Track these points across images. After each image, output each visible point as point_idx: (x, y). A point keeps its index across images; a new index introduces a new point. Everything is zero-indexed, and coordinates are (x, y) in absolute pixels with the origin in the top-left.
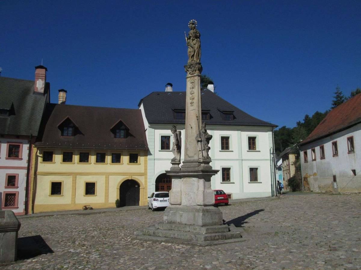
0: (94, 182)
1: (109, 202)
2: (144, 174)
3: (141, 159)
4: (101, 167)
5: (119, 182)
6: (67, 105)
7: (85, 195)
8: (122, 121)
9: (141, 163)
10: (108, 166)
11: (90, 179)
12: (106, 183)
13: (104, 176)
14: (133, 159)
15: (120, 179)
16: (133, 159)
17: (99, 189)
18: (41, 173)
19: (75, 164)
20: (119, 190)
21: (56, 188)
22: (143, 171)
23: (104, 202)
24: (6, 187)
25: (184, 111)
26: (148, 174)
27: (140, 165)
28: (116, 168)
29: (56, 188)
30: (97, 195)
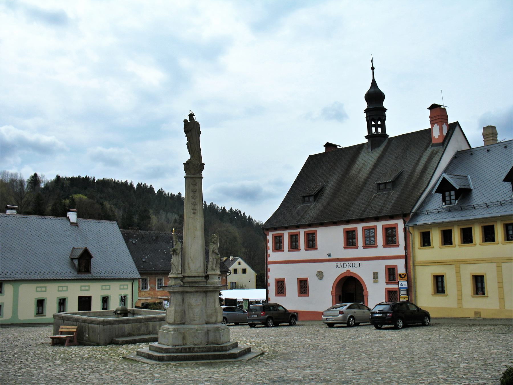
1: (506, 308)
11: (478, 270)
13: (494, 265)
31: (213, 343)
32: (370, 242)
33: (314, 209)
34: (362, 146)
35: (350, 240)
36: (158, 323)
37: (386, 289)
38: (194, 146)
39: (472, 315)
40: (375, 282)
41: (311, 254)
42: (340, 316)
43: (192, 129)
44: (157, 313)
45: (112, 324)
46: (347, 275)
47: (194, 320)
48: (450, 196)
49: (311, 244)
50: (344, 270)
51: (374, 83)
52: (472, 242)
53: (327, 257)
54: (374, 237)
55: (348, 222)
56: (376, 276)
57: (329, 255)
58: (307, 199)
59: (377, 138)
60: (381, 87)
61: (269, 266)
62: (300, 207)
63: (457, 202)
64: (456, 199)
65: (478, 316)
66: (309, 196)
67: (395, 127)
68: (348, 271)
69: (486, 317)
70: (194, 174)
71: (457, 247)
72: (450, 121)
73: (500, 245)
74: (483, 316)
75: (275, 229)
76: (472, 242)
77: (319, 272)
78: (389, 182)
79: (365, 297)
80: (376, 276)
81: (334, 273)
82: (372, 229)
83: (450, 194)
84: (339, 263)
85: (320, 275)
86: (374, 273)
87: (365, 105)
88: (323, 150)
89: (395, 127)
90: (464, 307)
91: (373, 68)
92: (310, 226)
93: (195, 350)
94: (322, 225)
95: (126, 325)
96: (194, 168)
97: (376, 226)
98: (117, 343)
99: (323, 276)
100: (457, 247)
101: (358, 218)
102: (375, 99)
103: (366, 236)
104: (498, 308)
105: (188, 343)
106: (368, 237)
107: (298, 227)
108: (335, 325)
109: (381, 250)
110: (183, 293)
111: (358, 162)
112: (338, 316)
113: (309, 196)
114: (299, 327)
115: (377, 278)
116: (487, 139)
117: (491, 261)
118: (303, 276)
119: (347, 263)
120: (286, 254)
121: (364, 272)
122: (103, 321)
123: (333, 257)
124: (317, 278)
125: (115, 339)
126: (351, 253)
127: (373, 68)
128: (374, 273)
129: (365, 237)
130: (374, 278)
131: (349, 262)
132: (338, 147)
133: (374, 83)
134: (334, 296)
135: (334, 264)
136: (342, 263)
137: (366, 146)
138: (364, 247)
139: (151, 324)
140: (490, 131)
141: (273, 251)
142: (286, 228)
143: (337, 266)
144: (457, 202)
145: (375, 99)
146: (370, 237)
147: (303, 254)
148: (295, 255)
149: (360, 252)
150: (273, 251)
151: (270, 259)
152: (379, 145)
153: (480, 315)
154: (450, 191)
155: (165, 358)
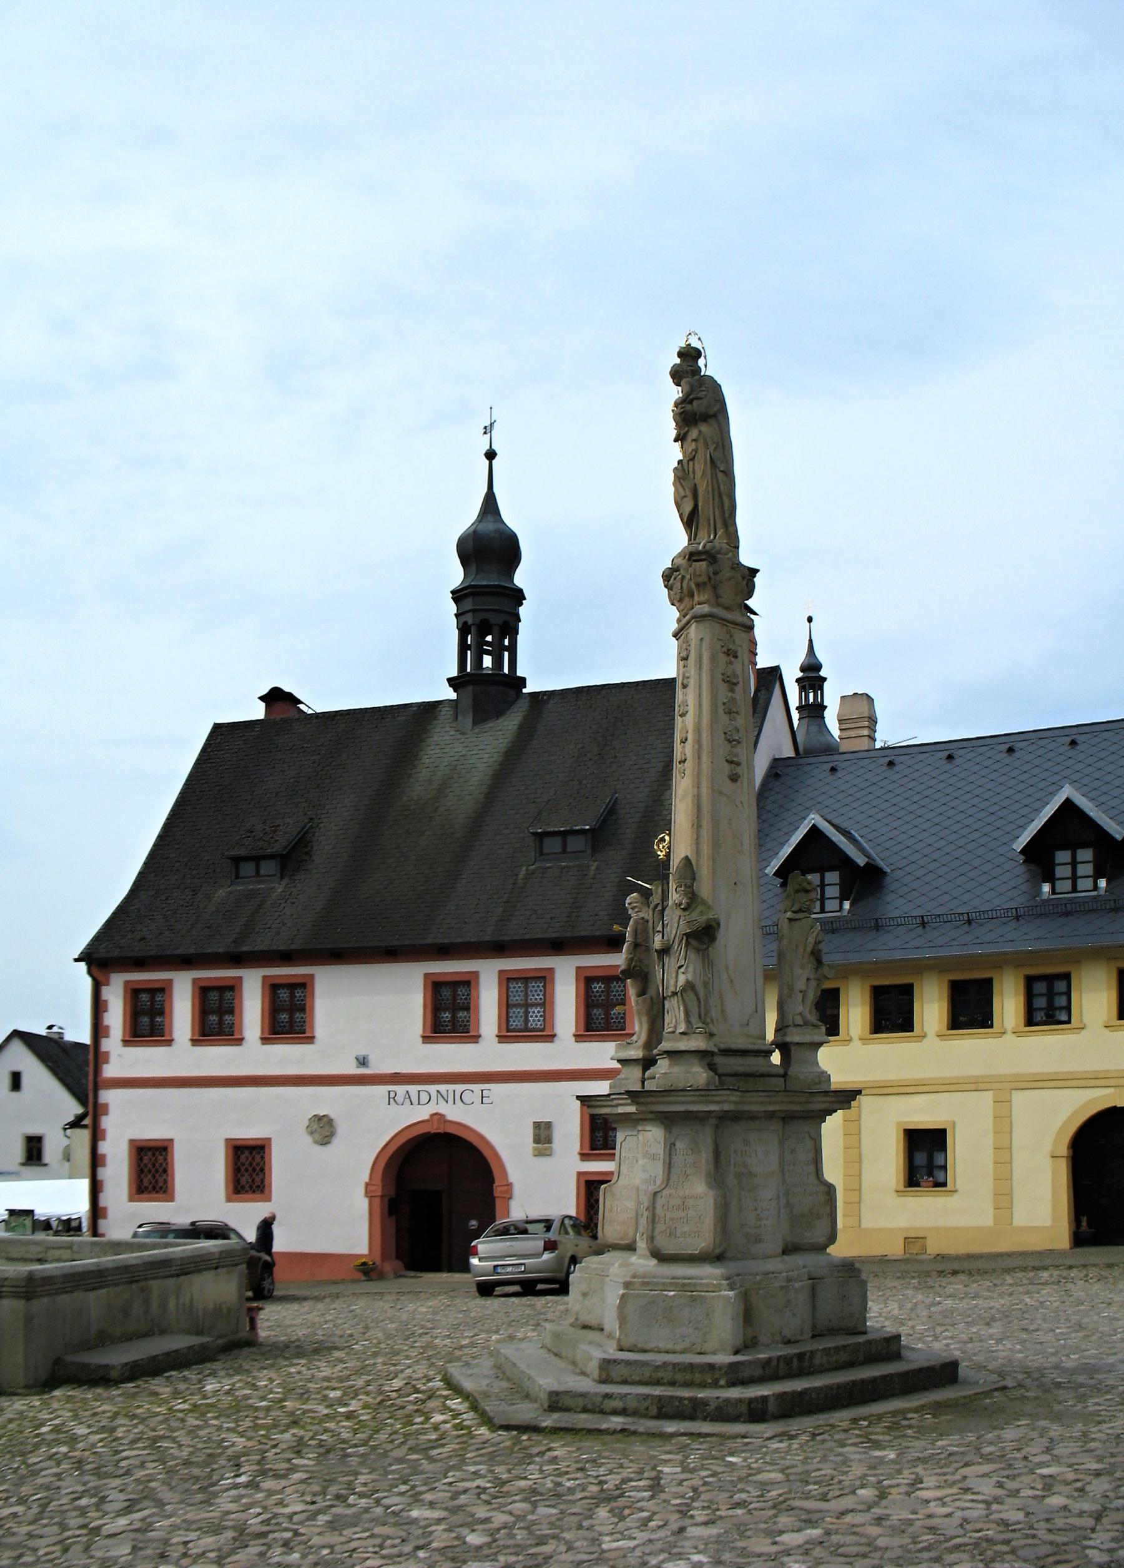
0: (901, 1135)
1: (1015, 1223)
4: (972, 1050)
5: (1065, 1125)
6: (893, 756)
7: (901, 1188)
8: (824, 826)
9: (1087, 1019)
10: (1010, 1045)
11: (924, 1113)
12: (997, 1132)
13: (988, 1096)
15: (1073, 1107)
17: (965, 1156)
18: (941, 1082)
19: (926, 1040)
20: (1063, 1169)
21: (925, 1155)
23: (989, 1222)
24: (584, 1157)
25: (844, 727)
27: (1083, 1032)
28: (1046, 1049)
29: (925, 1155)
30: (958, 1186)
31: (833, 1331)
32: (526, 1021)
33: (291, 906)
34: (431, 708)
35: (448, 1015)
36: (171, 1282)
37: (579, 1174)
38: (707, 489)
39: (895, 1249)
40: (539, 1154)
41: (286, 1057)
42: (547, 1256)
43: (701, 410)
44: (185, 1244)
45: (58, 1292)
46: (434, 1129)
47: (758, 1240)
48: (1074, 864)
49: (289, 1019)
50: (422, 1113)
51: (490, 505)
52: (910, 1028)
53: (353, 1070)
54: (543, 1005)
55: (444, 951)
56: (543, 1134)
57: (363, 1062)
58: (247, 869)
59: (487, 687)
60: (511, 517)
61: (108, 1096)
62: (222, 892)
63: (847, 905)
64: (843, 898)
65: (915, 1249)
66: (257, 859)
67: (549, 658)
68: (438, 1117)
69: (943, 1251)
70: (728, 609)
71: (856, 1043)
72: (763, 662)
73: (931, 1041)
74: (933, 1248)
75: (140, 964)
76: (910, 1028)
77: (319, 1118)
78: (582, 832)
79: (498, 1202)
80: (543, 1134)
81: (377, 1122)
82: (536, 978)
83: (1074, 857)
84: (401, 1089)
85: (323, 1129)
86: (537, 1125)
87: (455, 575)
88: (258, 711)
89: (549, 658)
90: (864, 1225)
91: (491, 455)
92: (287, 957)
93: (817, 1361)
94: (338, 956)
95: (92, 1295)
96: (713, 581)
97: (551, 971)
98: (100, 1378)
99: (332, 1134)
100: (856, 1043)
101: (487, 938)
102: (490, 552)
103: (513, 1000)
104: (989, 1222)
105: (763, 1339)
106: (516, 1006)
107: (237, 959)
108: (499, 1290)
109: (567, 1049)
110: (726, 1119)
111: (426, 760)
112: (539, 1255)
113: (257, 859)
114: (295, 1306)
115: (549, 1140)
116: (853, 733)
117: (976, 1085)
118: (249, 1132)
119: (432, 1088)
120: (182, 1054)
121: (497, 1122)
122: (31, 1278)
123: (379, 1066)
124: (308, 1139)
125: (69, 1358)
126: (451, 1056)
127: (491, 455)
128: (537, 1125)
129: (508, 1006)
130: (537, 1140)
131: (443, 1088)
132: (301, 706)
133: (490, 505)
134: (377, 1201)
135: (380, 1091)
136: (413, 1089)
137: (446, 713)
138: (502, 1039)
139: (156, 1285)
140: (862, 709)
141: (126, 1043)
142: (186, 962)
143: (392, 1098)
144: (847, 905)
145: (490, 552)
146: (527, 1005)
147: (253, 1053)
148: (217, 1059)
149: (489, 1051)
150: (126, 1043)
151: (110, 1071)
152: (499, 712)
153: (924, 1247)
154: (822, 870)
155: (772, 1407)
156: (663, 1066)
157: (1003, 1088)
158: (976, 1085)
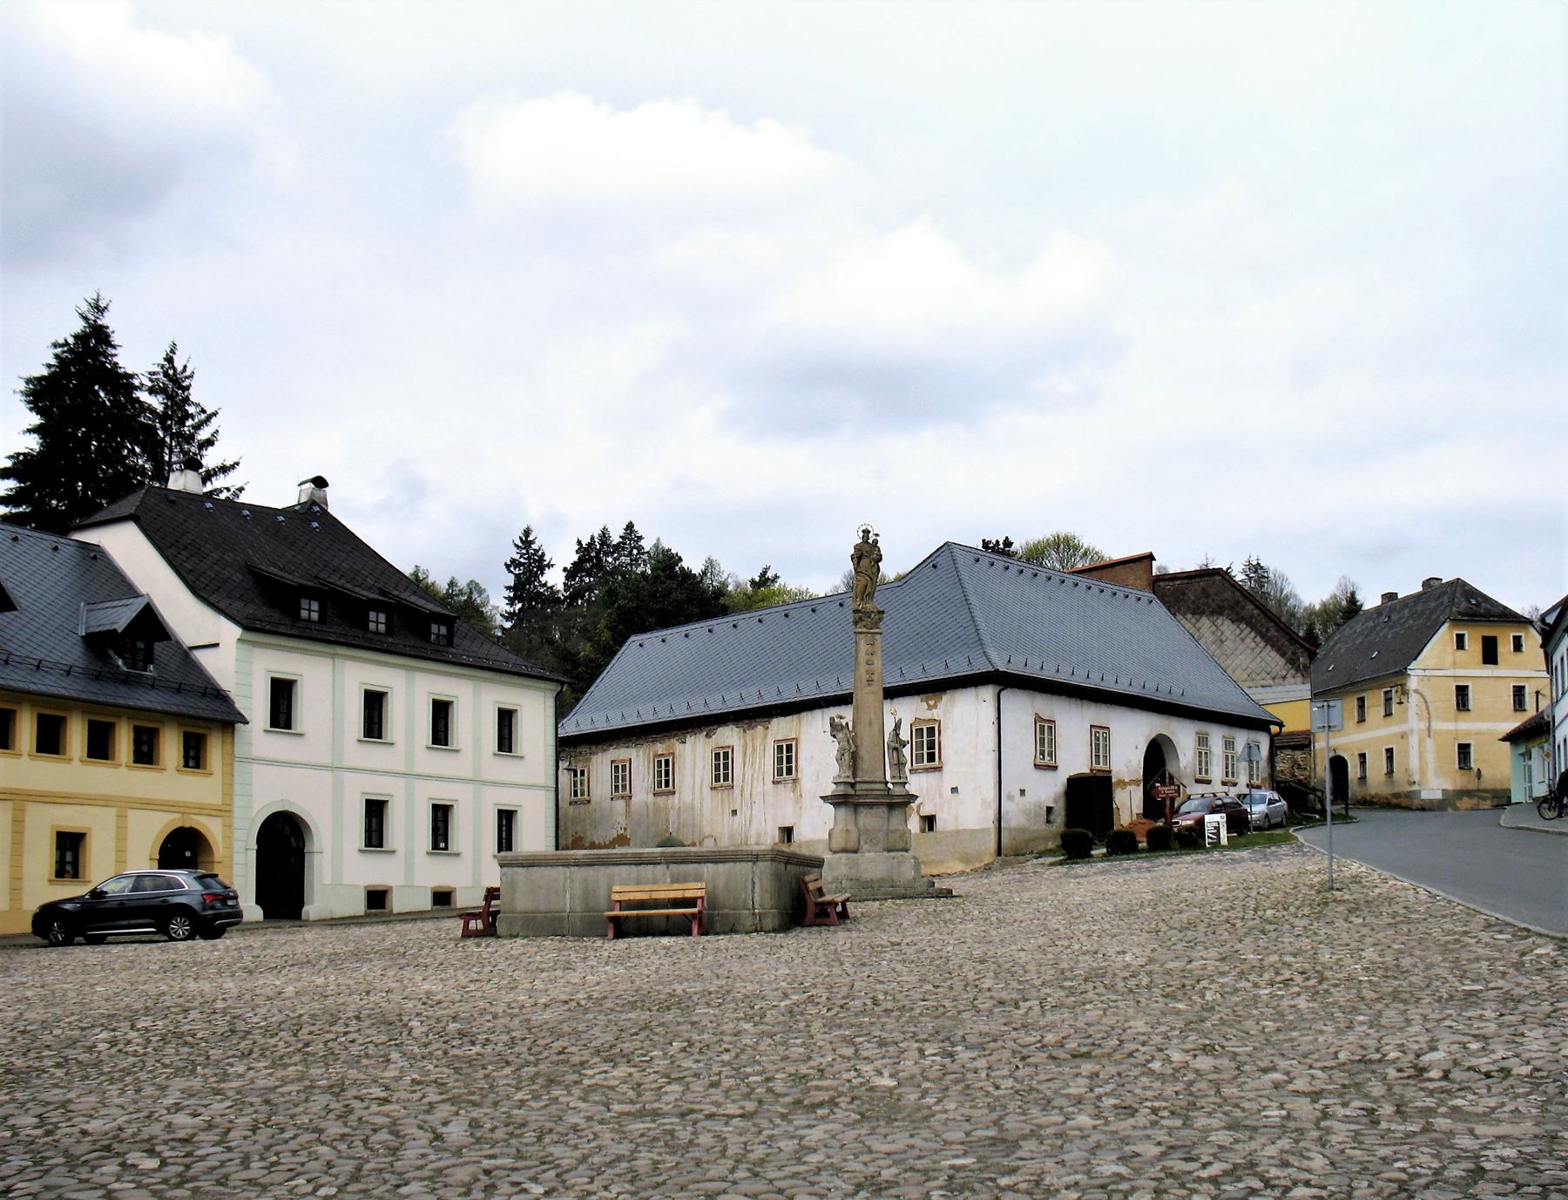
2: (223, 811)
3: (215, 751)
11: (71, 819)
14: (194, 757)
16: (194, 757)
22: (216, 799)
26: (237, 812)
117: (105, 802)
156: (858, 787)
157: (123, 805)
158: (105, 802)
